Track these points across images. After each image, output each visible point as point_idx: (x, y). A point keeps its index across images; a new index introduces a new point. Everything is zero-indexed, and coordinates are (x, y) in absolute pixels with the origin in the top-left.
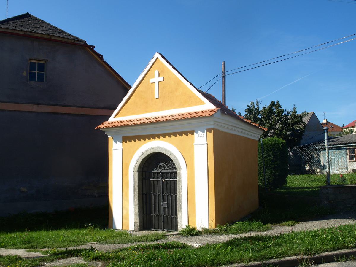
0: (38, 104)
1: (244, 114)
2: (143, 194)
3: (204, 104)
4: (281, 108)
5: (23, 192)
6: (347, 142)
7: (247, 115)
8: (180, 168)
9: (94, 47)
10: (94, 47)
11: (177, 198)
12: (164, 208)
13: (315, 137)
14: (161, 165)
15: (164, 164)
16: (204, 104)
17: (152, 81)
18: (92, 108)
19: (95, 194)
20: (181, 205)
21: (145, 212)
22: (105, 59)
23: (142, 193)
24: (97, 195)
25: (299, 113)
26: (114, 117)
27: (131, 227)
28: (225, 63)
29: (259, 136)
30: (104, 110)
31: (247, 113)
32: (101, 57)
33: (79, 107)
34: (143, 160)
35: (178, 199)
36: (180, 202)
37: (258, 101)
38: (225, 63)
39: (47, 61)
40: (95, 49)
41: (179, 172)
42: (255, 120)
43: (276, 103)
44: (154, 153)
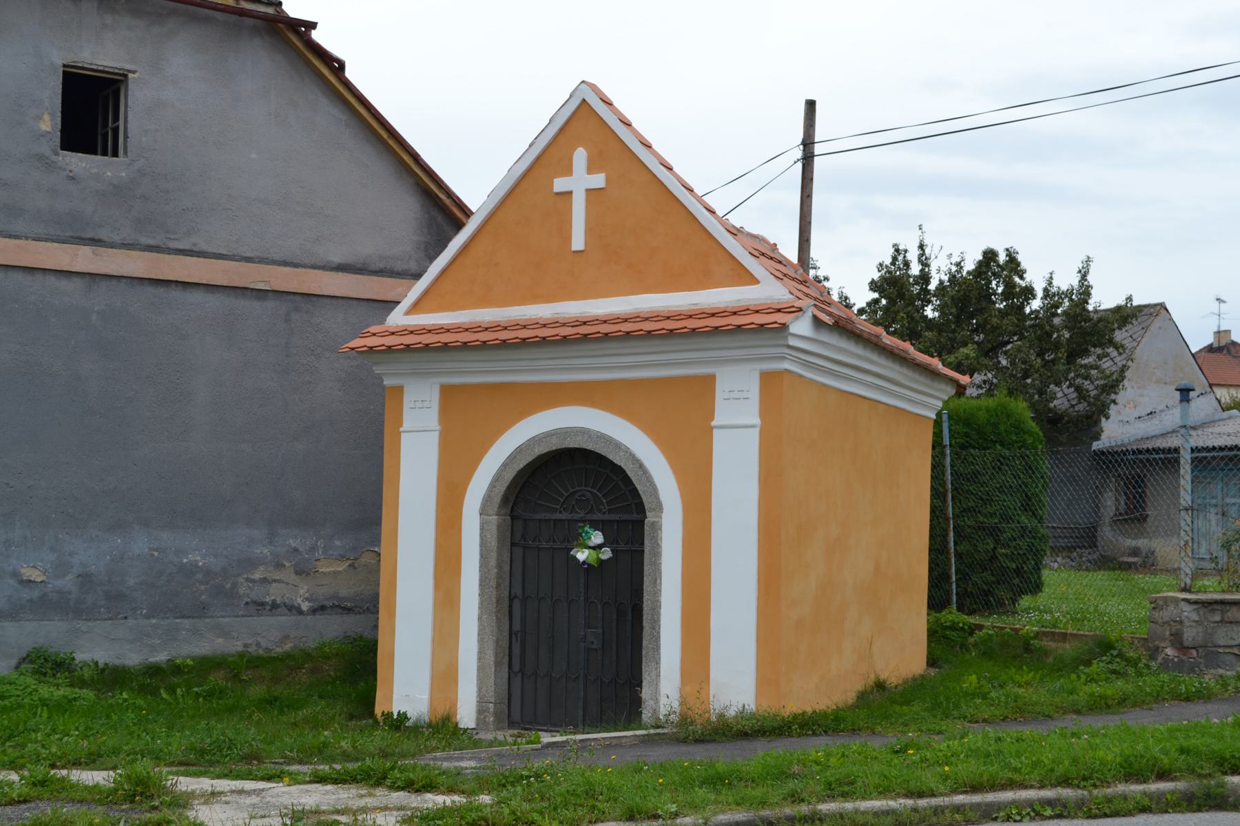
0: (95, 242)
1: (861, 297)
2: (511, 599)
3: (756, 282)
4: (1022, 278)
5: (30, 581)
6: (1211, 446)
7: (876, 301)
8: (659, 507)
9: (313, 25)
10: (313, 25)
11: (644, 612)
12: (589, 649)
13: (1162, 411)
14: (583, 495)
15: (595, 491)
16: (756, 282)
17: (560, 184)
18: (296, 265)
19: (299, 600)
20: (656, 639)
21: (516, 667)
22: (349, 74)
23: (510, 595)
24: (305, 606)
25: (1104, 298)
26: (408, 313)
27: (466, 716)
28: (811, 105)
29: (940, 404)
30: (340, 274)
31: (876, 295)
32: (338, 67)
33: (249, 260)
34: (521, 473)
35: (644, 617)
36: (654, 628)
37: (926, 242)
38: (811, 105)
39: (130, 75)
40: (316, 35)
41: (653, 524)
42: (914, 330)
43: (1002, 258)
44: (560, 449)
